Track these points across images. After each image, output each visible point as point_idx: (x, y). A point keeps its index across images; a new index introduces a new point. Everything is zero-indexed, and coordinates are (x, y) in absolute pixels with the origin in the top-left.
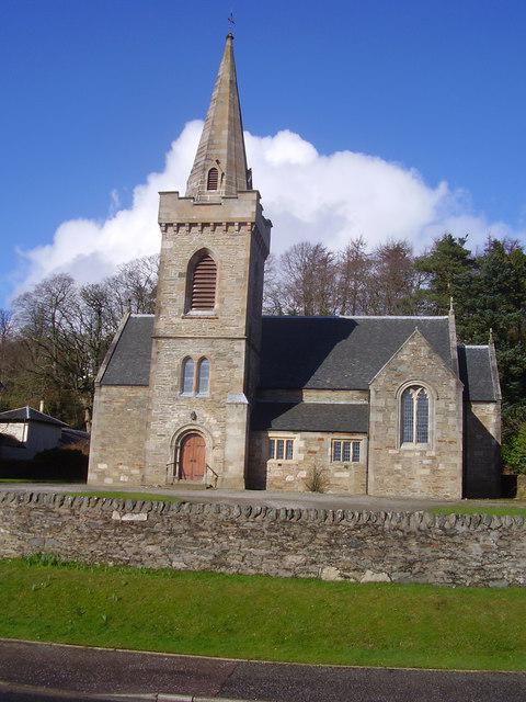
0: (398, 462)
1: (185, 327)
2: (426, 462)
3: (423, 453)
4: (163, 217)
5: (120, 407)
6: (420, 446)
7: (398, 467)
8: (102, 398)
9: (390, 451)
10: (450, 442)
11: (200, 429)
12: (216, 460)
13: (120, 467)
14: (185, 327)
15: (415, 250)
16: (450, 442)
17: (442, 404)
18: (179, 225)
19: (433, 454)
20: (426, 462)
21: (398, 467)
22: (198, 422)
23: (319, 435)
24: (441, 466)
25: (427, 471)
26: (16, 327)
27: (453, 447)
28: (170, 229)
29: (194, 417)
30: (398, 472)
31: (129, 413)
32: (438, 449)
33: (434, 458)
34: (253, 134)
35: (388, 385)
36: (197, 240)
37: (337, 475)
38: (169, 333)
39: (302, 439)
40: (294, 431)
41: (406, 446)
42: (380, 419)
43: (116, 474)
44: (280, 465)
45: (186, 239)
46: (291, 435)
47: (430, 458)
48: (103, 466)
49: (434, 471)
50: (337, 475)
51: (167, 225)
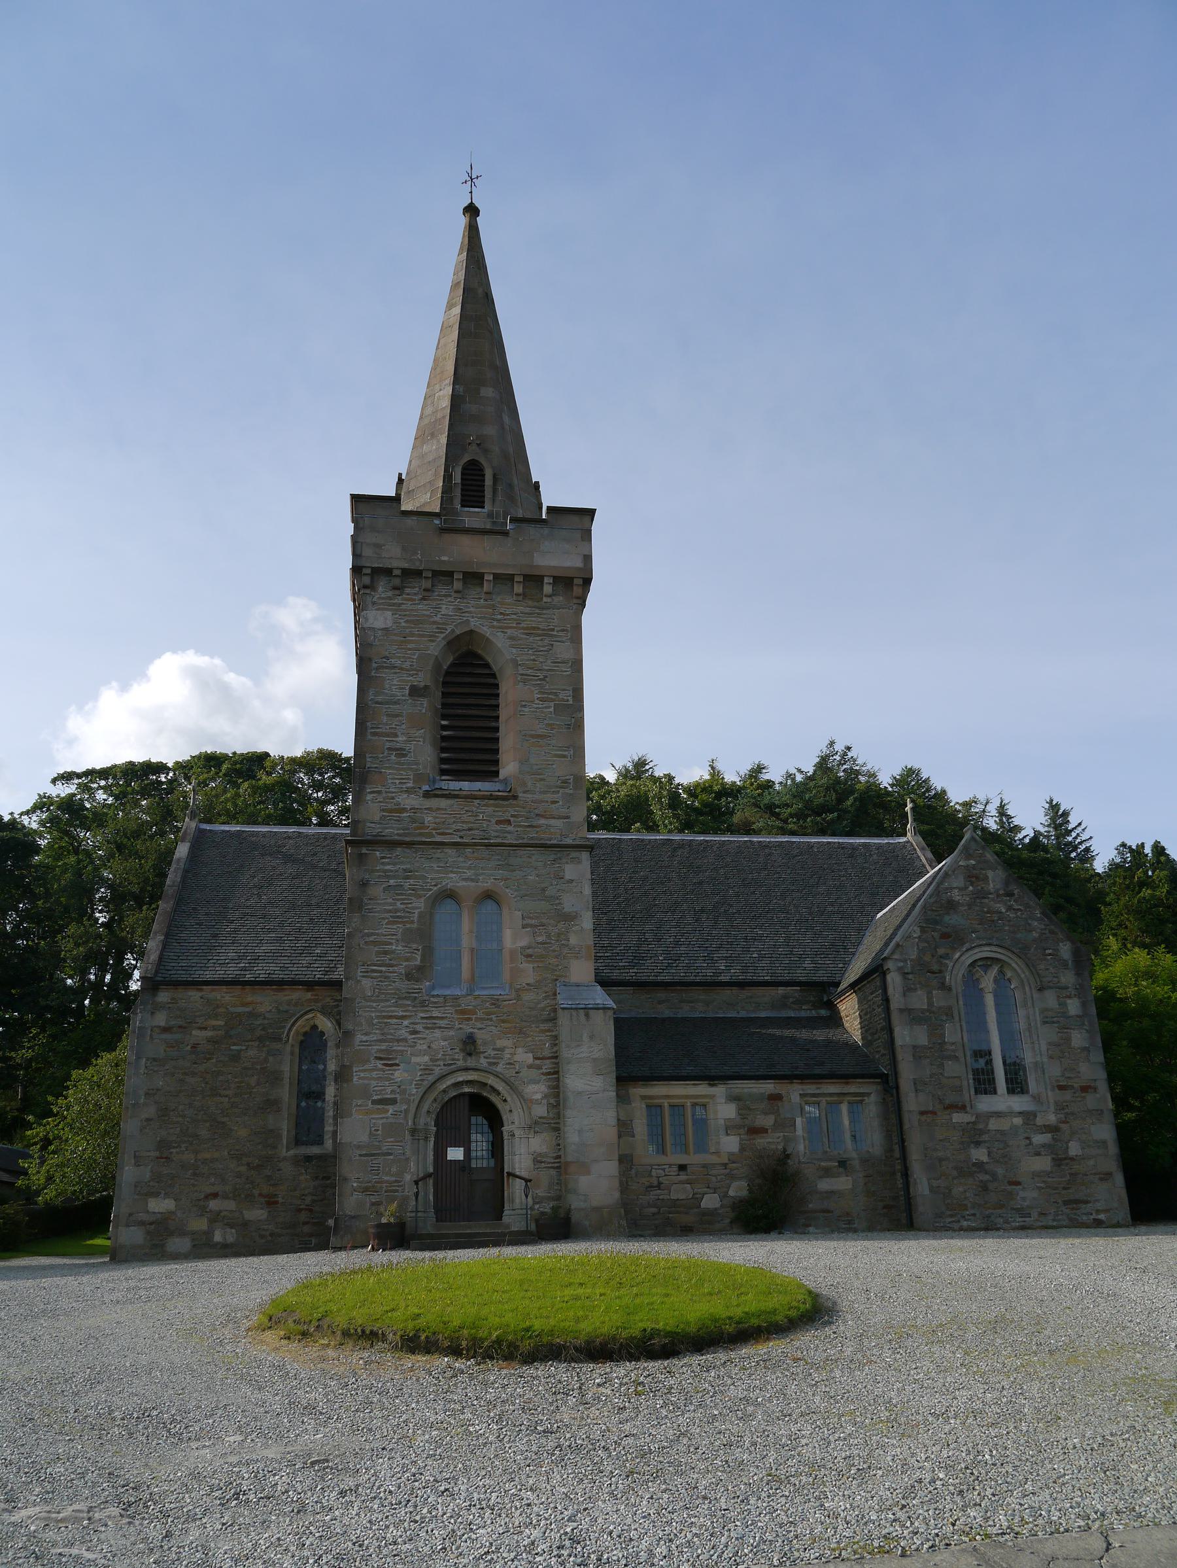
0: (978, 1144)
1: (438, 816)
2: (1039, 1139)
3: (1028, 1117)
4: (367, 552)
5: (209, 1040)
6: (1018, 1103)
7: (980, 1154)
8: (161, 1019)
9: (957, 1117)
10: (1085, 1089)
11: (491, 1081)
12: (537, 1160)
13: (213, 1205)
14: (438, 816)
15: (1095, 847)
16: (1085, 1089)
17: (1051, 999)
18: (408, 574)
19: (1052, 1118)
20: (1039, 1139)
21: (980, 1154)
22: (483, 1063)
23: (769, 1087)
24: (1074, 1149)
25: (1043, 1163)
26: (7, 818)
27: (1091, 1101)
28: (382, 589)
29: (469, 1045)
30: (980, 1165)
31: (236, 1058)
32: (1060, 1107)
33: (1052, 1129)
34: (1087, 856)
35: (927, 958)
36: (450, 612)
37: (824, 1185)
38: (392, 831)
39: (733, 1098)
40: (712, 1079)
41: (985, 1103)
42: (922, 1039)
43: (200, 1224)
44: (682, 1168)
45: (423, 608)
46: (702, 1089)
47: (1048, 1129)
48: (160, 1205)
49: (1061, 1160)
50: (824, 1185)
51: (377, 572)
